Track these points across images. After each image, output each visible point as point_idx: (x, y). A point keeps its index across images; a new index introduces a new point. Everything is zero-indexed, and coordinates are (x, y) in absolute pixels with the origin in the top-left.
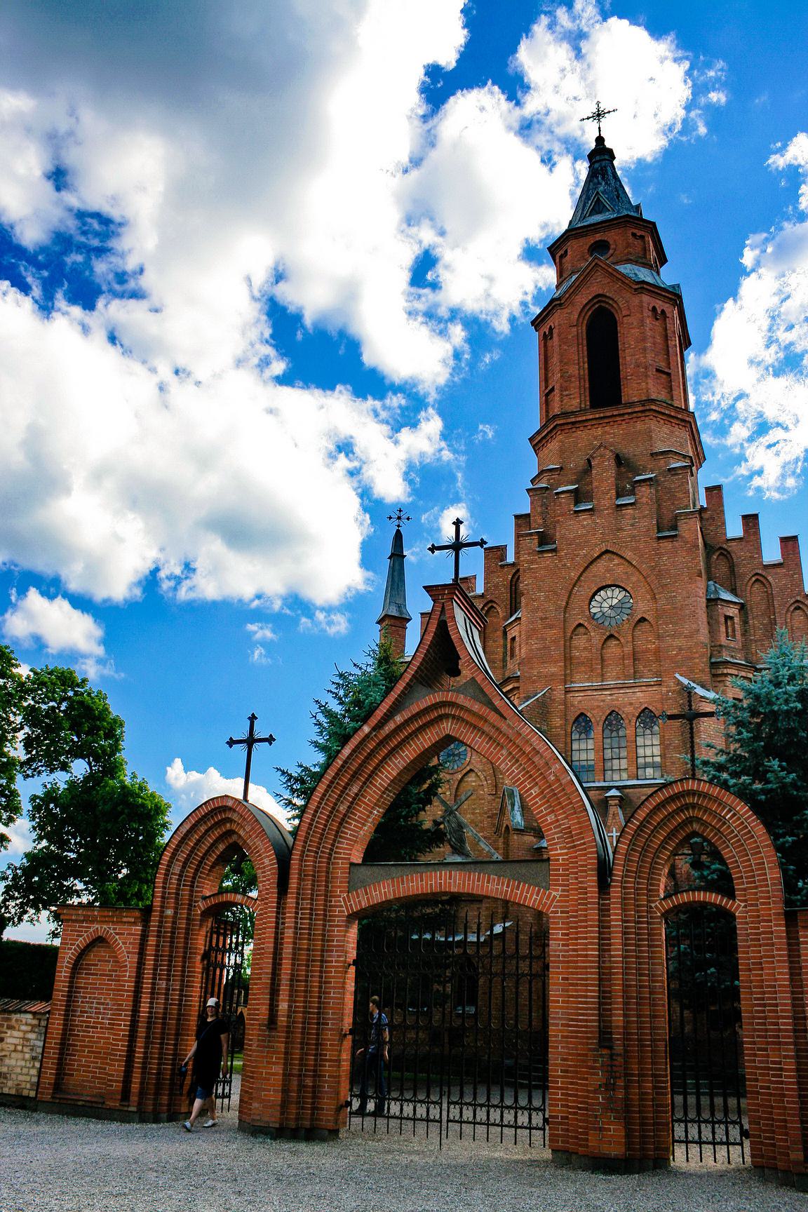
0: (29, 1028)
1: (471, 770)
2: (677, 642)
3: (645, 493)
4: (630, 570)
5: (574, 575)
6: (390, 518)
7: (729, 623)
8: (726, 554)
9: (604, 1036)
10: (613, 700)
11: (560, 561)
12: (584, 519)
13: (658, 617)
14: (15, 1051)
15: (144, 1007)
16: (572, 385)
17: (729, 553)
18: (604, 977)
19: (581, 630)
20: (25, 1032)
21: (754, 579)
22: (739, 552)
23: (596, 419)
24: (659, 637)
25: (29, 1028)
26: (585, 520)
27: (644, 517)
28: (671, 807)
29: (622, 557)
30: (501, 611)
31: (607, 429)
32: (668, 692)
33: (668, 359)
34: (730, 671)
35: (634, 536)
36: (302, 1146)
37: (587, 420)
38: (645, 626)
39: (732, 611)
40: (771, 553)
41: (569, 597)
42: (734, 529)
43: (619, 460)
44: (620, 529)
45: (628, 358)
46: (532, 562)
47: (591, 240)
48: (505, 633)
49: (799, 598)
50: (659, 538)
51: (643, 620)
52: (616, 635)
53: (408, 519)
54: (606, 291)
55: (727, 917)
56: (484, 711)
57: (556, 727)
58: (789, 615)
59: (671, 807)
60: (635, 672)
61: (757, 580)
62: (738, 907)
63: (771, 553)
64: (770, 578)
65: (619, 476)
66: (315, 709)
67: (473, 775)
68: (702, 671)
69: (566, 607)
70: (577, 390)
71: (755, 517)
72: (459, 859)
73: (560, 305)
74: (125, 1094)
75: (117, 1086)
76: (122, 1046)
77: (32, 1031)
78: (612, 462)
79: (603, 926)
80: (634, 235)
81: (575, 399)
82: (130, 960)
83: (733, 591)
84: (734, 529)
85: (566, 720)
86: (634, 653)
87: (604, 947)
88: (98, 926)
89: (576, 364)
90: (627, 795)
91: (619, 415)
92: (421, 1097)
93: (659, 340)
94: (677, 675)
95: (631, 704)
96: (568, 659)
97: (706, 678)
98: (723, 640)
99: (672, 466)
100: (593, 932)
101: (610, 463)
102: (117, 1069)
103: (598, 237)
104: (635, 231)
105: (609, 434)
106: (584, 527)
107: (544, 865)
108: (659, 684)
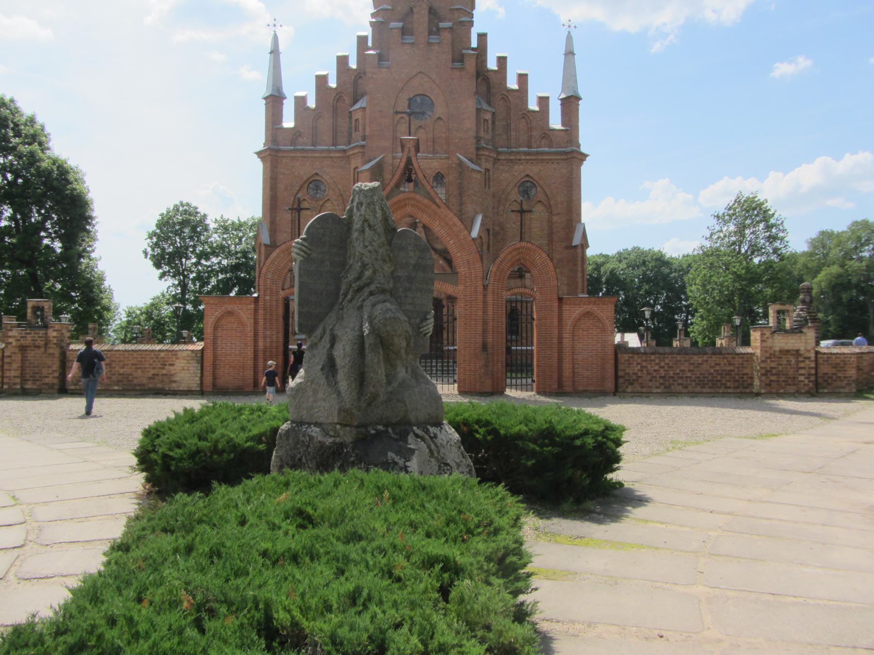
1: (328, 200)
3: (447, 36)
9: (485, 347)
14: (183, 369)
15: (261, 344)
18: (485, 322)
20: (188, 360)
29: (429, 77)
30: (347, 100)
34: (483, 153)
38: (441, 123)
41: (396, 99)
43: (432, 11)
48: (350, 117)
50: (452, 68)
51: (439, 118)
56: (430, 203)
60: (434, 150)
61: (503, 98)
65: (430, 21)
67: (330, 202)
71: (547, 98)
75: (250, 381)
76: (250, 363)
78: (426, 12)
79: (485, 302)
82: (249, 323)
87: (485, 311)
92: (524, 376)
94: (458, 154)
95: (431, 169)
98: (482, 134)
100: (481, 305)
102: (249, 374)
108: (448, 158)
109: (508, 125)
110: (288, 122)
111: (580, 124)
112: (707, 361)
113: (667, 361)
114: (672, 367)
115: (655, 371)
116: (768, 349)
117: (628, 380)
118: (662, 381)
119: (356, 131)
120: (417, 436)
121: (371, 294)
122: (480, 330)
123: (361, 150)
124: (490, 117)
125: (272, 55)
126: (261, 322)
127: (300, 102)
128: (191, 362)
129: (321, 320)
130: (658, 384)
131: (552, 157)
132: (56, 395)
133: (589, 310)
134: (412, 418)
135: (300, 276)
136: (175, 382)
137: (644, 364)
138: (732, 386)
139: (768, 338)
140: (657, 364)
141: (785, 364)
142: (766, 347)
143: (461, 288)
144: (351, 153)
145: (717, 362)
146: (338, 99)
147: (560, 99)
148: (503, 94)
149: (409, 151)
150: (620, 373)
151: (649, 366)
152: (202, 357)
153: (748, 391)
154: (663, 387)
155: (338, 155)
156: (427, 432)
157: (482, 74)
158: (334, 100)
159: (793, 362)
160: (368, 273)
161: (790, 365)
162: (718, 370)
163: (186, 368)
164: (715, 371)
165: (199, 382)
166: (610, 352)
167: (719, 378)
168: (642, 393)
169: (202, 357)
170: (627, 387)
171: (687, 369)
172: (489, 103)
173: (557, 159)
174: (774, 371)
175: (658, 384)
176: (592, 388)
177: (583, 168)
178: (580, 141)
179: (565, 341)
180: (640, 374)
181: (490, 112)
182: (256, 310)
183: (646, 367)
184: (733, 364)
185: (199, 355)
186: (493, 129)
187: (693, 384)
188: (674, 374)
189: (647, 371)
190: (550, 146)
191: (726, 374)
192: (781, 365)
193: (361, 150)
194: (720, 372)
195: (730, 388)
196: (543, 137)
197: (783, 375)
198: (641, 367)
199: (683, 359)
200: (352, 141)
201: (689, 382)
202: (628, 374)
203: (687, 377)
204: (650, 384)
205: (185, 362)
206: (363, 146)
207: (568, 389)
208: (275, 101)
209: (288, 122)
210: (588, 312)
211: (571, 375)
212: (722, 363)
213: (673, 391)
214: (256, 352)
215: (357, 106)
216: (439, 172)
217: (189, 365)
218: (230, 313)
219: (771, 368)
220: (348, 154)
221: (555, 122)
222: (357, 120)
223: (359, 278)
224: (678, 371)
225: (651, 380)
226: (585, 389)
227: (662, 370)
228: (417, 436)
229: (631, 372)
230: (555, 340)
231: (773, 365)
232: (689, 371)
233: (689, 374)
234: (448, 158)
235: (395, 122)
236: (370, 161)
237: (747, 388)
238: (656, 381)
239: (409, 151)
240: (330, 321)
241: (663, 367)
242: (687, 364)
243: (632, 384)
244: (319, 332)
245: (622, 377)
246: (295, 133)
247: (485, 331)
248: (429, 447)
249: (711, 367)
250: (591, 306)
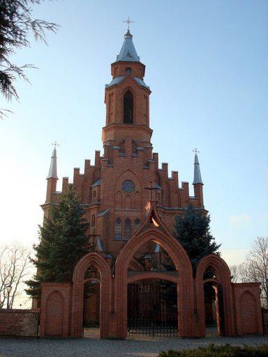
9: (196, 312)
15: (73, 310)
26: (122, 159)
36: (120, 341)
42: (160, 167)
47: (126, 66)
74: (69, 334)
81: (120, 120)
87: (195, 292)
89: (118, 104)
101: (130, 142)
102: (66, 327)
103: (128, 66)
110: (59, 188)
126: (74, 297)
127: (65, 180)
132: (260, 261)
136: (23, 331)
143: (180, 279)
157: (158, 173)
166: (259, 312)
169: (39, 317)
172: (160, 185)
182: (71, 291)
208: (52, 181)
209: (59, 188)
214: (70, 314)
215: (96, 184)
221: (192, 193)
246: (62, 195)
247: (195, 302)
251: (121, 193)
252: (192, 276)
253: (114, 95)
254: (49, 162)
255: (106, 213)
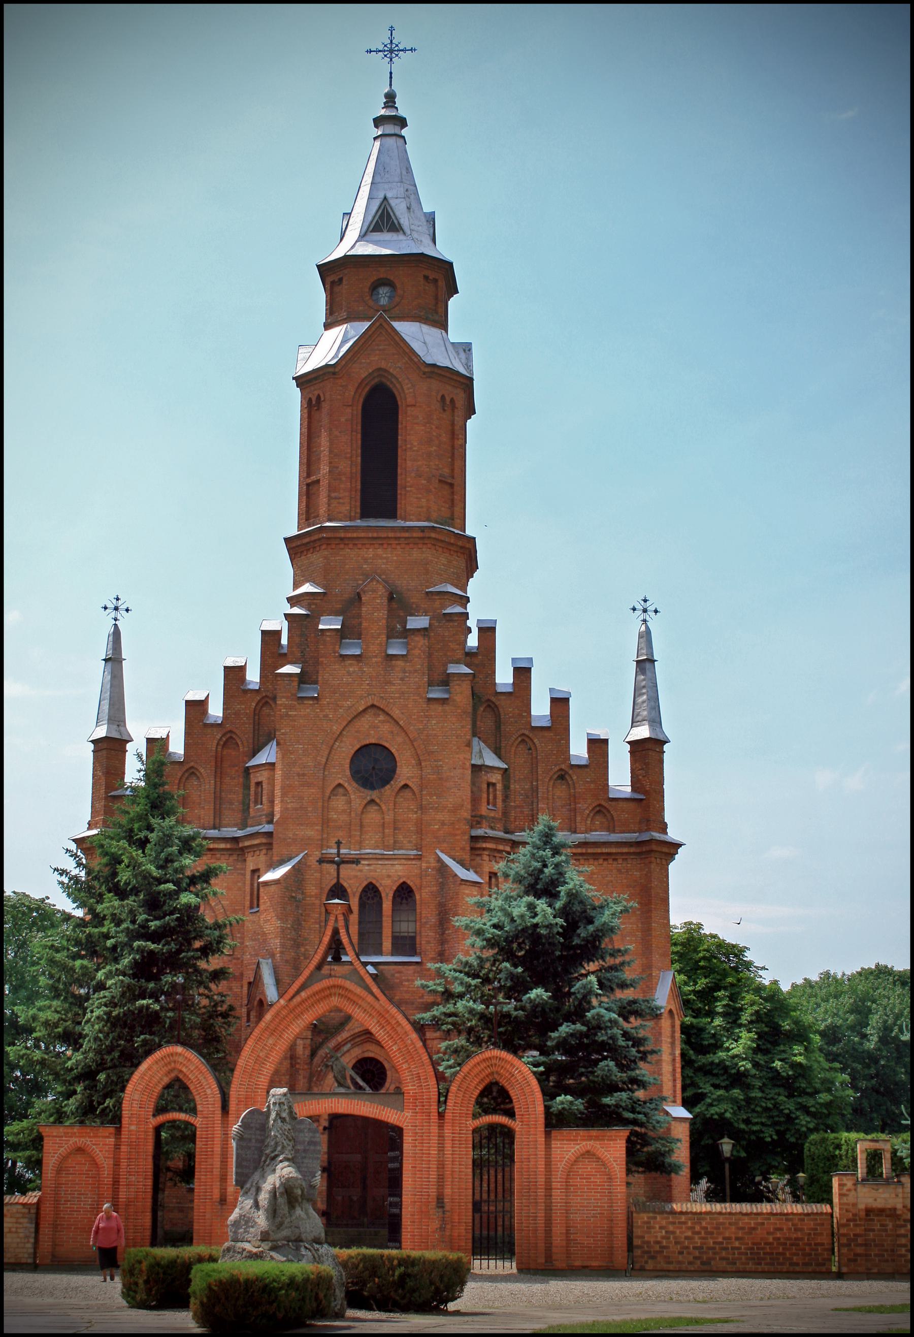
0: (21, 1215)
2: (440, 816)
4: (396, 729)
5: (336, 728)
6: (105, 608)
7: (491, 790)
8: (492, 707)
9: (440, 1202)
10: (370, 871)
11: (322, 711)
12: (351, 665)
13: (422, 787)
16: (342, 486)
17: (496, 706)
18: (441, 1165)
19: (341, 790)
20: (18, 1218)
21: (520, 739)
22: (507, 709)
23: (368, 538)
24: (422, 808)
25: (21, 1215)
27: (416, 671)
28: (483, 1066)
29: (388, 714)
31: (380, 551)
32: (428, 868)
33: (452, 464)
34: (484, 845)
35: (403, 693)
37: (358, 538)
38: (407, 793)
39: (496, 778)
40: (540, 708)
42: (504, 676)
44: (390, 683)
45: (409, 463)
46: (291, 708)
49: (563, 766)
51: (406, 786)
52: (378, 801)
53: (127, 610)
54: (383, 365)
55: (508, 1134)
57: (311, 896)
58: (551, 783)
59: (483, 1066)
60: (395, 842)
61: (523, 741)
62: (515, 1125)
63: (540, 708)
64: (535, 741)
66: (56, 876)
68: (463, 849)
69: (326, 763)
70: (347, 494)
72: (342, 1090)
73: (334, 373)
77: (23, 1217)
78: (385, 601)
80: (426, 278)
83: (498, 752)
84: (504, 676)
85: (321, 888)
86: (395, 821)
87: (441, 1149)
88: (77, 1140)
90: (381, 972)
91: (396, 538)
93: (445, 438)
95: (389, 876)
96: (326, 822)
97: (467, 857)
98: (484, 810)
99: (448, 611)
103: (382, 273)
104: (428, 273)
105: (382, 558)
106: (349, 674)
107: (401, 1097)
108: (419, 858)
109: (535, 790)
111: (666, 787)
112: (763, 1224)
113: (704, 1224)
114: (712, 1233)
115: (687, 1238)
116: (850, 1207)
117: (649, 1252)
118: (697, 1253)
119: (256, 803)
120: (306, 1248)
121: (281, 1161)
122: (433, 1176)
123: (264, 840)
124: (499, 777)
125: (109, 664)
127: (156, 745)
128: (21, 1220)
129: (249, 1177)
130: (691, 1258)
131: (614, 850)
133: (589, 1148)
134: (303, 1236)
135: (237, 1149)
137: (671, 1228)
138: (800, 1262)
139: (849, 1190)
140: (689, 1228)
141: (879, 1230)
142: (848, 1204)
144: (247, 843)
145: (778, 1226)
146: (225, 743)
147: (628, 742)
148: (523, 734)
149: (336, 920)
150: (637, 1242)
151: (678, 1231)
152: (38, 1214)
153: (824, 1269)
154: (698, 1262)
155: (222, 846)
156: (313, 1246)
158: (218, 744)
159: (890, 1226)
160: (279, 1148)
161: (886, 1230)
162: (779, 1239)
163: (14, 1230)
164: (774, 1239)
165: (32, 1251)
167: (781, 1250)
168: (669, 1271)
169: (38, 1214)
170: (646, 1262)
171: (733, 1236)
173: (622, 854)
174: (860, 1240)
175: (691, 1258)
176: (595, 1263)
177: (672, 867)
178: (667, 819)
179: (554, 1192)
180: (664, 1243)
181: (498, 769)
182: (117, 1146)
183: (673, 1233)
184: (801, 1230)
185: (33, 1211)
186: (506, 798)
187: (743, 1257)
188: (714, 1243)
189: (675, 1238)
190: (611, 829)
191: (791, 1245)
192: (873, 1230)
193: (264, 840)
194: (782, 1240)
195: (797, 1264)
196: (599, 811)
197: (876, 1245)
198: (666, 1232)
199: (727, 1221)
200: (250, 822)
201: (736, 1255)
202: (648, 1242)
203: (733, 1248)
204: (680, 1258)
205: (14, 1220)
206: (269, 834)
207: (558, 1264)
210: (588, 1152)
211: (564, 1243)
212: (785, 1227)
213: (715, 1269)
216: (404, 883)
217: (18, 1225)
218: (80, 1150)
219: (855, 1235)
220: (241, 845)
222: (259, 784)
223: (272, 1152)
224: (720, 1240)
225: (681, 1253)
226: (585, 1264)
227: (696, 1237)
228: (306, 1248)
229: (652, 1240)
230: (541, 1192)
231: (858, 1231)
232: (737, 1239)
233: (737, 1244)
234: (419, 858)
235: (327, 795)
236: (281, 863)
237: (824, 1264)
238: (689, 1253)
239: (336, 920)
240: (256, 1176)
241: (699, 1233)
242: (733, 1228)
243: (653, 1258)
244: (248, 1186)
245: (638, 1247)
247: (441, 1178)
248: (313, 1255)
249: (768, 1233)
250: (592, 1142)
251: (346, 794)
252: (219, 1112)
253: (325, 406)
254: (97, 671)
255: (299, 862)
